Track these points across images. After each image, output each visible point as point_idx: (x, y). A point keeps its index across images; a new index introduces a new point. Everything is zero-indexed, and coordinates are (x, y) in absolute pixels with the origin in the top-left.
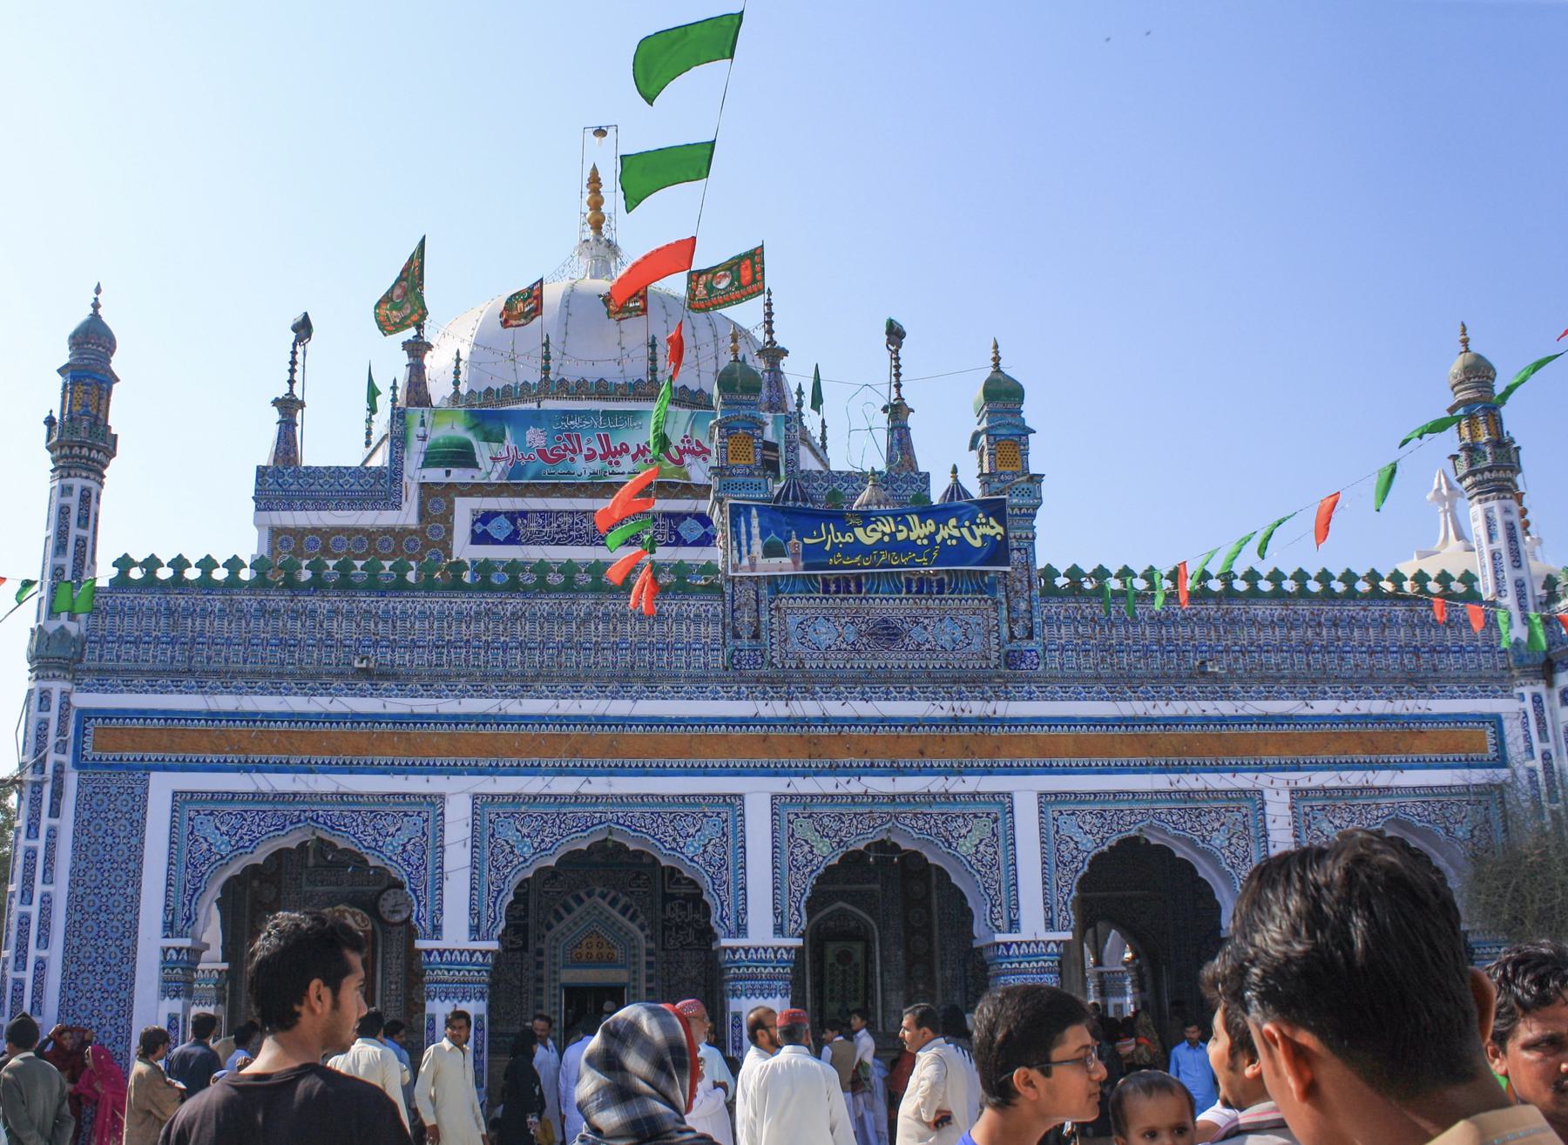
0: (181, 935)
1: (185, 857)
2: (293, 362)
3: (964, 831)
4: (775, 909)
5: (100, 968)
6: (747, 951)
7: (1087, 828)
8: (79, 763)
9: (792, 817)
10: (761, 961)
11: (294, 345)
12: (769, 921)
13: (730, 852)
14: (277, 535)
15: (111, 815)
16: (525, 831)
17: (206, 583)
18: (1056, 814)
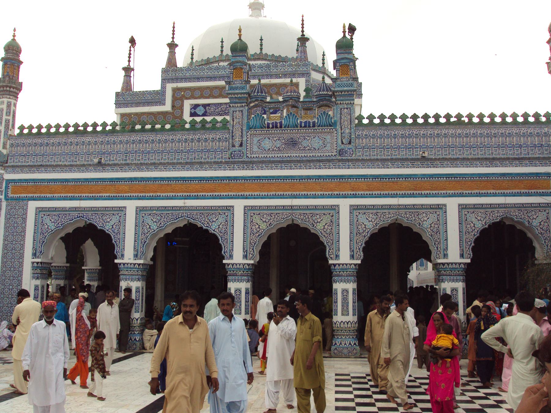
0: (38, 257)
1: (40, 231)
2: (130, 54)
3: (319, 220)
4: (244, 249)
5: (12, 269)
6: (233, 265)
7: (370, 219)
8: (7, 198)
9: (252, 214)
10: (238, 269)
11: (130, 47)
12: (458, 252)
13: (228, 228)
14: (123, 116)
15: (16, 216)
16: (154, 220)
17: (48, 133)
18: (357, 214)
